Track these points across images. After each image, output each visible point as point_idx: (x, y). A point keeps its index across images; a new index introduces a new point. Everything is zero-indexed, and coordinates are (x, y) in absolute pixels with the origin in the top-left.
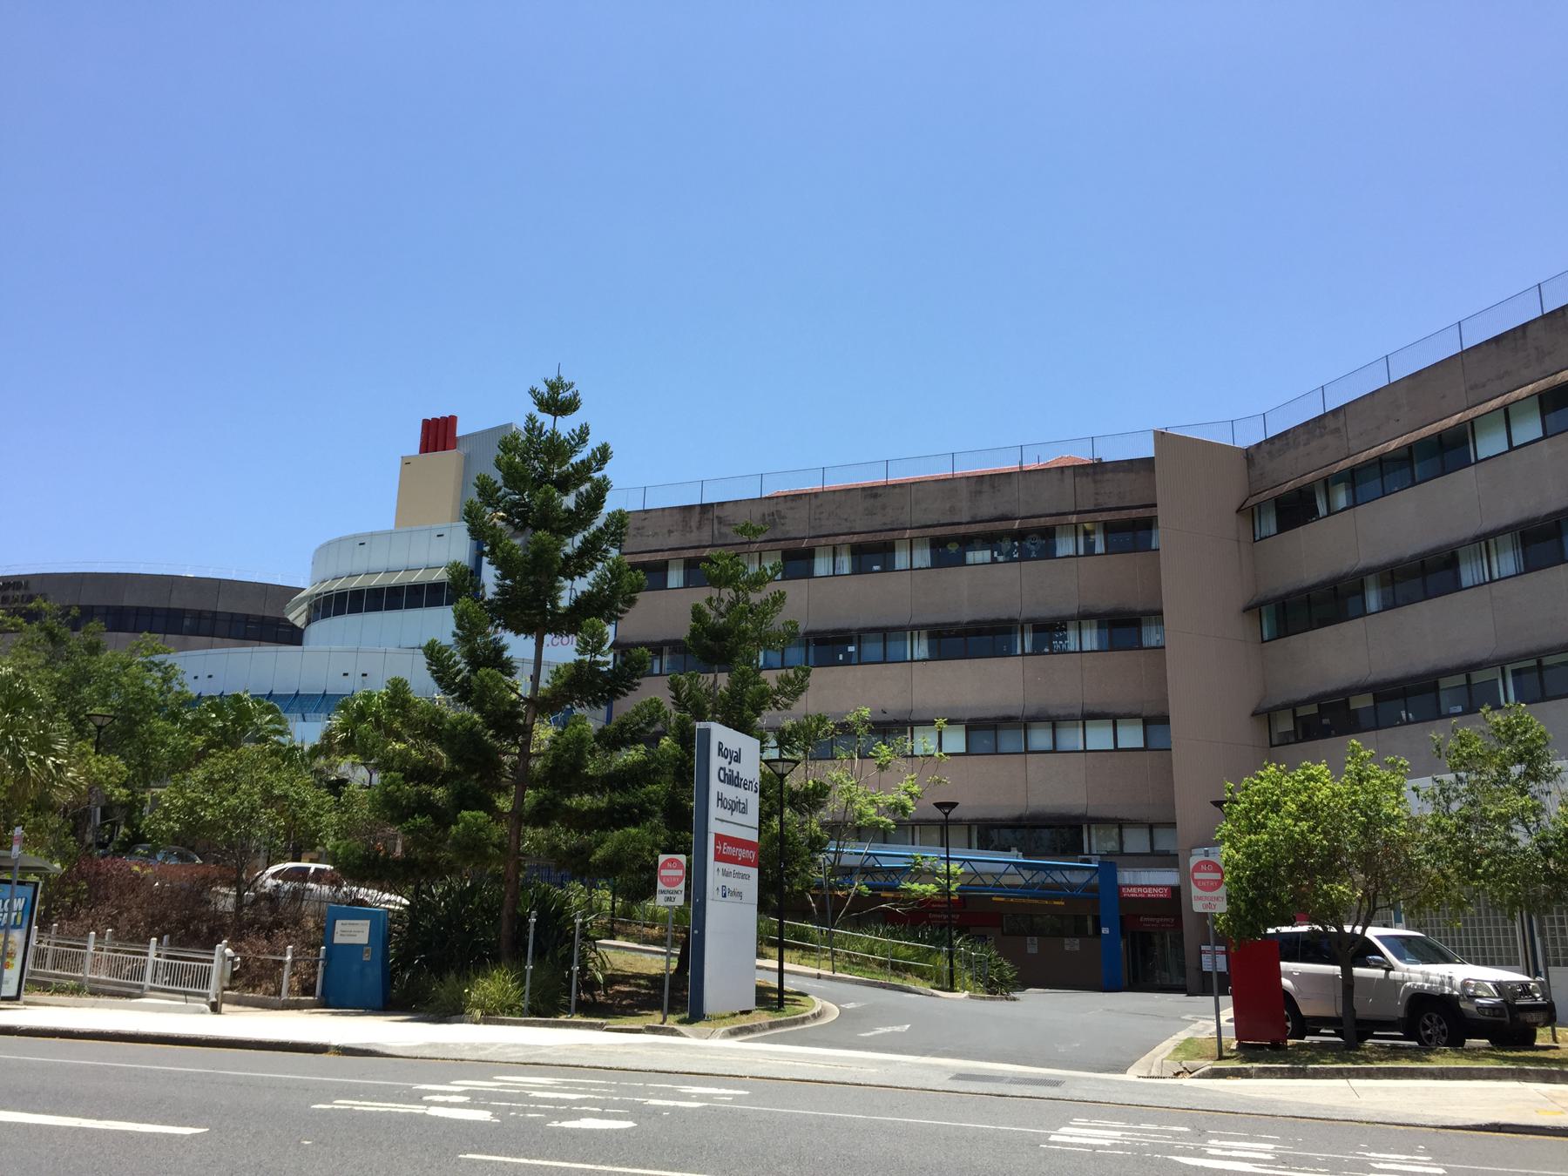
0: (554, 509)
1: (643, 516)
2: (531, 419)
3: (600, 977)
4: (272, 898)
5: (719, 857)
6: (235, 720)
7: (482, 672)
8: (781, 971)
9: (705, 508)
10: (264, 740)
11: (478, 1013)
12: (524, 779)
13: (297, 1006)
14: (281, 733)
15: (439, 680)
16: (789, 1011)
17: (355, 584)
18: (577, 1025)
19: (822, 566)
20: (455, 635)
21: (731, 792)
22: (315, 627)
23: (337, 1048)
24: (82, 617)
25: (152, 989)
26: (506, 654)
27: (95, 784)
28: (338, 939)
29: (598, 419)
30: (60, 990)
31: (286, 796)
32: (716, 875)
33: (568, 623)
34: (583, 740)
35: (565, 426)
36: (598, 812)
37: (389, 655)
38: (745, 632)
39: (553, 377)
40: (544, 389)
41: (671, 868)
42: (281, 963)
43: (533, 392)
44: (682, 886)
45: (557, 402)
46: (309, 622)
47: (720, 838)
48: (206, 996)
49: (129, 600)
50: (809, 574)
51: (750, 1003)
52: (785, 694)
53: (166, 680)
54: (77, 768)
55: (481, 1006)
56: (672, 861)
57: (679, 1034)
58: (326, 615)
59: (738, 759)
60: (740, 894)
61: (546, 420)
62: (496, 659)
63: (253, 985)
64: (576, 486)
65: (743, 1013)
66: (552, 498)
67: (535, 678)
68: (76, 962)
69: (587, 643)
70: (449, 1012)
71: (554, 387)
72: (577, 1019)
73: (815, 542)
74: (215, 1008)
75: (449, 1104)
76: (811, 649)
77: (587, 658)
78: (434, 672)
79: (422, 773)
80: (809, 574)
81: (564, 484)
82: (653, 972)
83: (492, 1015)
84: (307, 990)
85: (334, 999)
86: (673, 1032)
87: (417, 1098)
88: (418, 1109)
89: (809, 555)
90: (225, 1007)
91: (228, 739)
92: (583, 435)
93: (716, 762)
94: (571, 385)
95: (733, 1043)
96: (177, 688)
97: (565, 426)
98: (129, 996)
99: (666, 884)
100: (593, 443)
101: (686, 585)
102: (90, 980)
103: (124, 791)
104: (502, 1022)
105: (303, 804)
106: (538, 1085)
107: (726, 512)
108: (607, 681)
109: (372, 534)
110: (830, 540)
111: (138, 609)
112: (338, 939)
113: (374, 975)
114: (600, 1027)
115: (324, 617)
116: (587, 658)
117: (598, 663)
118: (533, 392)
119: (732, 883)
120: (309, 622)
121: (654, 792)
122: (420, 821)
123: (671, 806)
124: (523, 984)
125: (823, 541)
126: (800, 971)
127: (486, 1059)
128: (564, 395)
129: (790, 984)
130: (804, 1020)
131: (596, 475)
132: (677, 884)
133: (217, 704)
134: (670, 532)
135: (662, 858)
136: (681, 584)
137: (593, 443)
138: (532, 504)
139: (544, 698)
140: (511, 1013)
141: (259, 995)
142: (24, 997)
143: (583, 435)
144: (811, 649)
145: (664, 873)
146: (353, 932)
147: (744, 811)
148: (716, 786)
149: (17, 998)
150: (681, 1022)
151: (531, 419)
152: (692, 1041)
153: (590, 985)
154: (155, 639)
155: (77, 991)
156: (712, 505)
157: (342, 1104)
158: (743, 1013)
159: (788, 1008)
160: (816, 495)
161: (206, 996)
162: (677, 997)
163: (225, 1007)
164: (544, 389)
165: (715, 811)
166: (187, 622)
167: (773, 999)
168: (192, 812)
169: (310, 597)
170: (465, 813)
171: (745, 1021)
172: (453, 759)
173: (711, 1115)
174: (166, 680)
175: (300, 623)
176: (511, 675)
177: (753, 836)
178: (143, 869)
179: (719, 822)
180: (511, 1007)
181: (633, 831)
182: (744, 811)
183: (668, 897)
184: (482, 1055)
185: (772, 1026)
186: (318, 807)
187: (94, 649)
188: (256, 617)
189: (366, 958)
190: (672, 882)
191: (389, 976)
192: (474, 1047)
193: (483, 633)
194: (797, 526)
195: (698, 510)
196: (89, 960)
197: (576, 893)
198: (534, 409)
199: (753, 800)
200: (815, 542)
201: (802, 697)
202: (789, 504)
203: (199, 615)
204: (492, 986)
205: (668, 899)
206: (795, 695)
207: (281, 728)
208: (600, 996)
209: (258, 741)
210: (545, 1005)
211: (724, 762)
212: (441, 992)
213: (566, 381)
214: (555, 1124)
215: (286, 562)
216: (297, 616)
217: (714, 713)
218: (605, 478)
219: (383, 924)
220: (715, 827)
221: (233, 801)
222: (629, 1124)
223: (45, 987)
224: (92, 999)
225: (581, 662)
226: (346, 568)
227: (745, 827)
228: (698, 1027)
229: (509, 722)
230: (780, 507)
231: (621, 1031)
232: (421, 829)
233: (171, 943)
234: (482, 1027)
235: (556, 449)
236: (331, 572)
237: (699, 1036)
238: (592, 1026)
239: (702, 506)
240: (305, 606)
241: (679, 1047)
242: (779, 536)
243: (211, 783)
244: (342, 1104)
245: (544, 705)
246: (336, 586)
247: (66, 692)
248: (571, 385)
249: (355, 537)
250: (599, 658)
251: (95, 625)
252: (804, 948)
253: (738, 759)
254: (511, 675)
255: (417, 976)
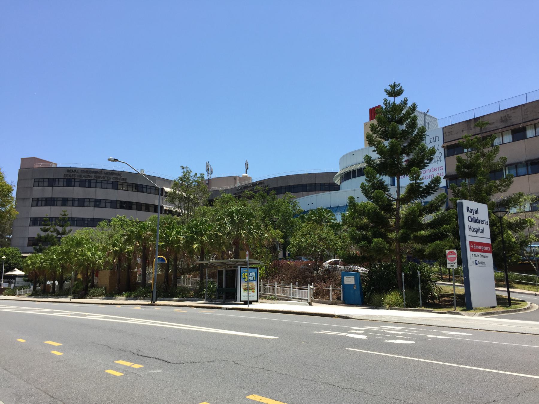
0: (396, 131)
1: (451, 127)
2: (385, 100)
3: (436, 295)
4: (328, 270)
5: (472, 250)
6: (320, 216)
7: (376, 191)
8: (509, 292)
9: (476, 119)
10: (328, 222)
11: (388, 306)
12: (398, 227)
13: (335, 303)
14: (334, 220)
15: (366, 196)
16: (513, 307)
17: (353, 168)
18: (423, 311)
19: (530, 133)
20: (366, 180)
21: (475, 225)
22: (343, 184)
23: (337, 316)
24: (280, 190)
25: (293, 298)
26: (385, 184)
27: (274, 239)
28: (346, 283)
29: (410, 96)
30: (269, 299)
31: (325, 238)
32: (471, 256)
33: (406, 171)
34: (415, 211)
35: (398, 100)
36: (429, 236)
37: (353, 190)
38: (480, 164)
39: (392, 84)
40: (389, 88)
41: (451, 255)
42: (329, 290)
43: (386, 91)
44: (456, 261)
45: (395, 92)
46: (341, 183)
47: (471, 243)
48: (307, 300)
49: (291, 183)
50: (525, 137)
51: (495, 303)
52: (503, 186)
53: (294, 206)
54: (272, 234)
55: (389, 304)
56: (451, 252)
57: (461, 314)
58: (345, 180)
59: (477, 212)
60: (484, 263)
61: (391, 100)
62: (382, 187)
63: (320, 296)
64: (405, 121)
65: (491, 307)
66: (395, 127)
67: (398, 192)
68: (272, 290)
69: (413, 177)
70: (378, 305)
71: (393, 87)
72: (423, 308)
73: (525, 124)
74: (310, 304)
75: (357, 334)
76: (529, 168)
77: (414, 182)
78: (364, 193)
79: (361, 228)
80: (525, 137)
81: (400, 121)
82: (461, 293)
83: (392, 307)
84: (339, 299)
85: (347, 302)
86: (458, 314)
87: (347, 331)
88: (344, 334)
89: (524, 130)
90: (313, 303)
91: (319, 221)
92: (406, 100)
93: (466, 214)
94: (399, 85)
95: (483, 318)
96: (298, 208)
97: (398, 100)
98: (287, 300)
99: (450, 260)
100: (409, 104)
101: (513, 141)
102: (277, 296)
103: (283, 240)
104: (396, 309)
105: (331, 240)
106: (391, 329)
107: (486, 120)
108: (424, 189)
109: (356, 151)
110: (533, 122)
111: (294, 185)
112: (346, 283)
113: (358, 293)
114: (431, 311)
115: (348, 179)
116: (414, 182)
117: (419, 183)
118: (386, 91)
119: (479, 259)
120: (341, 183)
121: (447, 228)
122: (363, 243)
123: (450, 230)
124: (403, 297)
125: (529, 123)
126: (518, 292)
127: (395, 320)
128: (397, 89)
129: (513, 297)
130: (519, 310)
131: (412, 115)
132: (454, 260)
133: (314, 212)
134: (463, 131)
135: (447, 251)
136: (511, 140)
137: (409, 104)
138: (395, 129)
139: (402, 198)
140: (399, 306)
141: (324, 300)
142: (259, 301)
143: (406, 100)
144: (529, 168)
145: (449, 256)
146: (350, 280)
147: (482, 232)
148: (467, 224)
149: (257, 301)
150: (462, 310)
151: (385, 100)
152: (466, 317)
153: (434, 298)
154: (291, 195)
155: (273, 299)
156: (479, 118)
157: (322, 332)
158: (491, 307)
159: (513, 306)
160: (524, 105)
161: (307, 300)
162: (464, 303)
163: (313, 303)
164: (389, 88)
165: (468, 233)
166: (308, 188)
167: (505, 303)
168: (299, 244)
169: (340, 175)
170: (374, 239)
171: (491, 310)
172: (374, 221)
173: (451, 341)
174: (294, 206)
175: (339, 184)
176: (388, 191)
177: (489, 241)
178: (291, 262)
179: (470, 237)
180: (399, 304)
181: (438, 242)
182: (482, 232)
183: (452, 264)
184: (383, 319)
185: (503, 312)
186: (336, 241)
187: (273, 199)
188: (324, 183)
189: (355, 288)
190: (452, 260)
191: (363, 295)
192: (381, 317)
193: (375, 178)
194: (517, 120)
195: (473, 121)
196: (276, 290)
197: (426, 267)
198: (387, 97)
199: (487, 228)
200: (525, 124)
201: (511, 186)
202: (513, 111)
203: (311, 185)
204: (392, 297)
205: (452, 266)
206: (508, 186)
207: (333, 218)
208: (437, 301)
209: (326, 222)
210: (411, 304)
211: (471, 214)
212: (376, 297)
213: (397, 83)
214: (386, 341)
215: (330, 164)
216: (337, 181)
217: (470, 196)
218: (415, 115)
219: (360, 279)
220: (468, 239)
221: (310, 241)
222: (413, 342)
223: (266, 298)
224: (277, 301)
225: (413, 183)
226: (349, 163)
227: (485, 237)
228: (469, 312)
229: (387, 207)
230: (508, 113)
231: (439, 313)
232: (364, 246)
233: (299, 284)
234: (389, 311)
235: (396, 109)
236: (345, 165)
237: (469, 315)
238: (428, 311)
239: (475, 119)
240: (339, 178)
241: (463, 319)
242: (509, 124)
243: (304, 235)
244: (322, 332)
245: (403, 201)
246: (347, 170)
247: (267, 213)
248: (399, 85)
249: (351, 153)
250: (418, 181)
251: (273, 192)
252: (531, 284)
253: (477, 212)
254: (388, 191)
255: (369, 295)
